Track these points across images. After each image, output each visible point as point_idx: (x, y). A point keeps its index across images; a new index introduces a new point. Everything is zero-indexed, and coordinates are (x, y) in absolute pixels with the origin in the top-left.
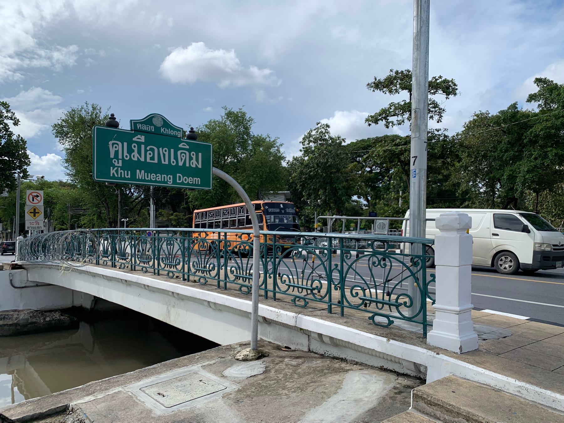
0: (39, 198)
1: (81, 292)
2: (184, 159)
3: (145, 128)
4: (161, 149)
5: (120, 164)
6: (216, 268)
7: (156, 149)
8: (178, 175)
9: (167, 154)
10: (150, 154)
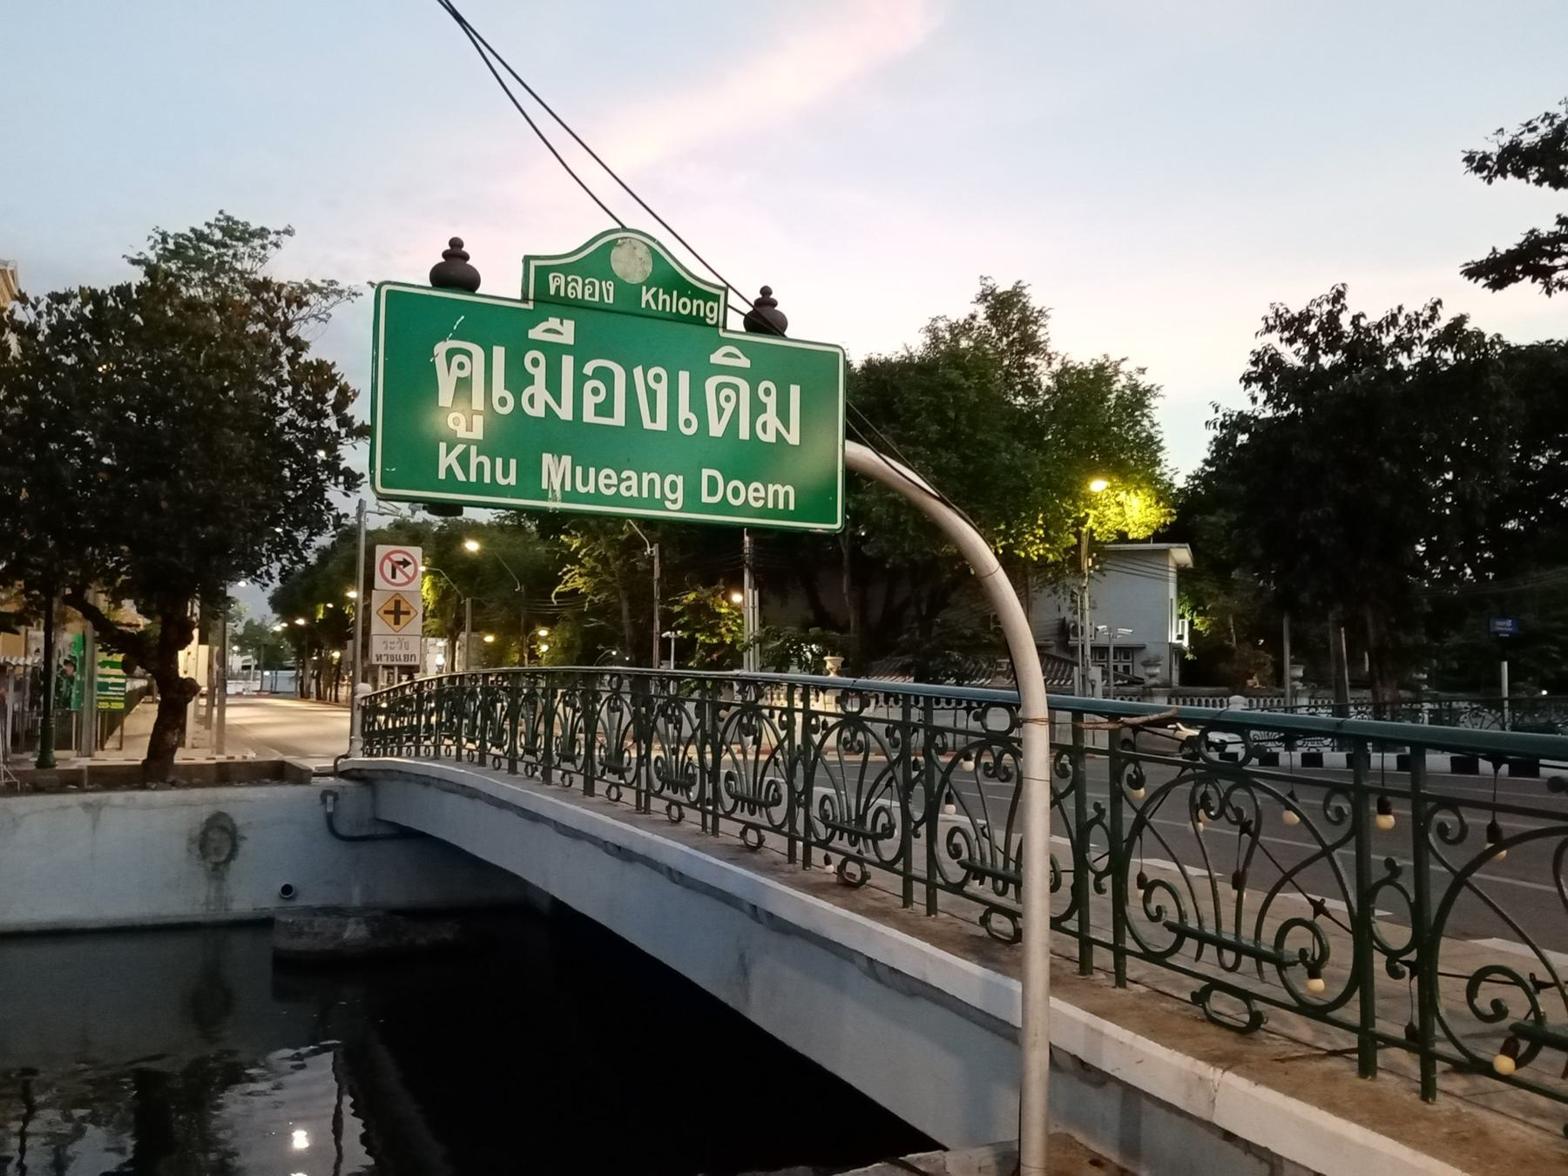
0: (409, 570)
1: (505, 871)
2: (729, 408)
3: (578, 289)
4: (638, 372)
5: (478, 434)
6: (897, 833)
7: (619, 372)
8: (706, 473)
9: (662, 390)
10: (595, 391)
